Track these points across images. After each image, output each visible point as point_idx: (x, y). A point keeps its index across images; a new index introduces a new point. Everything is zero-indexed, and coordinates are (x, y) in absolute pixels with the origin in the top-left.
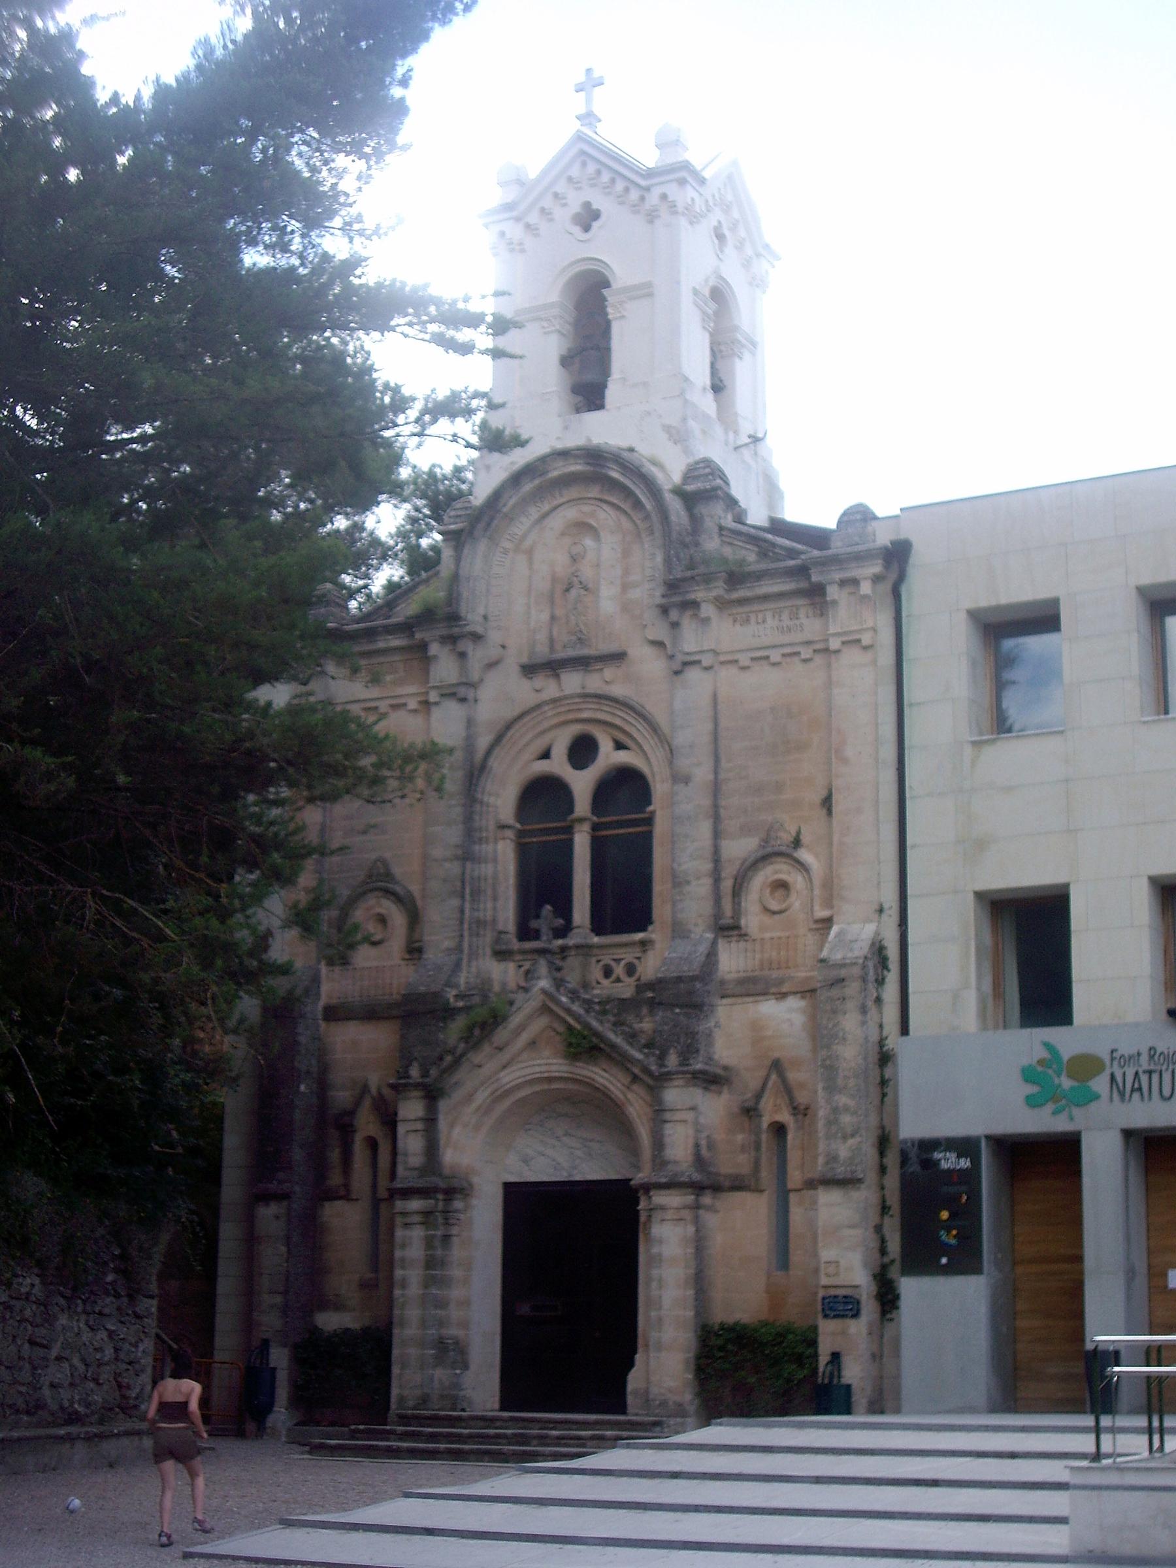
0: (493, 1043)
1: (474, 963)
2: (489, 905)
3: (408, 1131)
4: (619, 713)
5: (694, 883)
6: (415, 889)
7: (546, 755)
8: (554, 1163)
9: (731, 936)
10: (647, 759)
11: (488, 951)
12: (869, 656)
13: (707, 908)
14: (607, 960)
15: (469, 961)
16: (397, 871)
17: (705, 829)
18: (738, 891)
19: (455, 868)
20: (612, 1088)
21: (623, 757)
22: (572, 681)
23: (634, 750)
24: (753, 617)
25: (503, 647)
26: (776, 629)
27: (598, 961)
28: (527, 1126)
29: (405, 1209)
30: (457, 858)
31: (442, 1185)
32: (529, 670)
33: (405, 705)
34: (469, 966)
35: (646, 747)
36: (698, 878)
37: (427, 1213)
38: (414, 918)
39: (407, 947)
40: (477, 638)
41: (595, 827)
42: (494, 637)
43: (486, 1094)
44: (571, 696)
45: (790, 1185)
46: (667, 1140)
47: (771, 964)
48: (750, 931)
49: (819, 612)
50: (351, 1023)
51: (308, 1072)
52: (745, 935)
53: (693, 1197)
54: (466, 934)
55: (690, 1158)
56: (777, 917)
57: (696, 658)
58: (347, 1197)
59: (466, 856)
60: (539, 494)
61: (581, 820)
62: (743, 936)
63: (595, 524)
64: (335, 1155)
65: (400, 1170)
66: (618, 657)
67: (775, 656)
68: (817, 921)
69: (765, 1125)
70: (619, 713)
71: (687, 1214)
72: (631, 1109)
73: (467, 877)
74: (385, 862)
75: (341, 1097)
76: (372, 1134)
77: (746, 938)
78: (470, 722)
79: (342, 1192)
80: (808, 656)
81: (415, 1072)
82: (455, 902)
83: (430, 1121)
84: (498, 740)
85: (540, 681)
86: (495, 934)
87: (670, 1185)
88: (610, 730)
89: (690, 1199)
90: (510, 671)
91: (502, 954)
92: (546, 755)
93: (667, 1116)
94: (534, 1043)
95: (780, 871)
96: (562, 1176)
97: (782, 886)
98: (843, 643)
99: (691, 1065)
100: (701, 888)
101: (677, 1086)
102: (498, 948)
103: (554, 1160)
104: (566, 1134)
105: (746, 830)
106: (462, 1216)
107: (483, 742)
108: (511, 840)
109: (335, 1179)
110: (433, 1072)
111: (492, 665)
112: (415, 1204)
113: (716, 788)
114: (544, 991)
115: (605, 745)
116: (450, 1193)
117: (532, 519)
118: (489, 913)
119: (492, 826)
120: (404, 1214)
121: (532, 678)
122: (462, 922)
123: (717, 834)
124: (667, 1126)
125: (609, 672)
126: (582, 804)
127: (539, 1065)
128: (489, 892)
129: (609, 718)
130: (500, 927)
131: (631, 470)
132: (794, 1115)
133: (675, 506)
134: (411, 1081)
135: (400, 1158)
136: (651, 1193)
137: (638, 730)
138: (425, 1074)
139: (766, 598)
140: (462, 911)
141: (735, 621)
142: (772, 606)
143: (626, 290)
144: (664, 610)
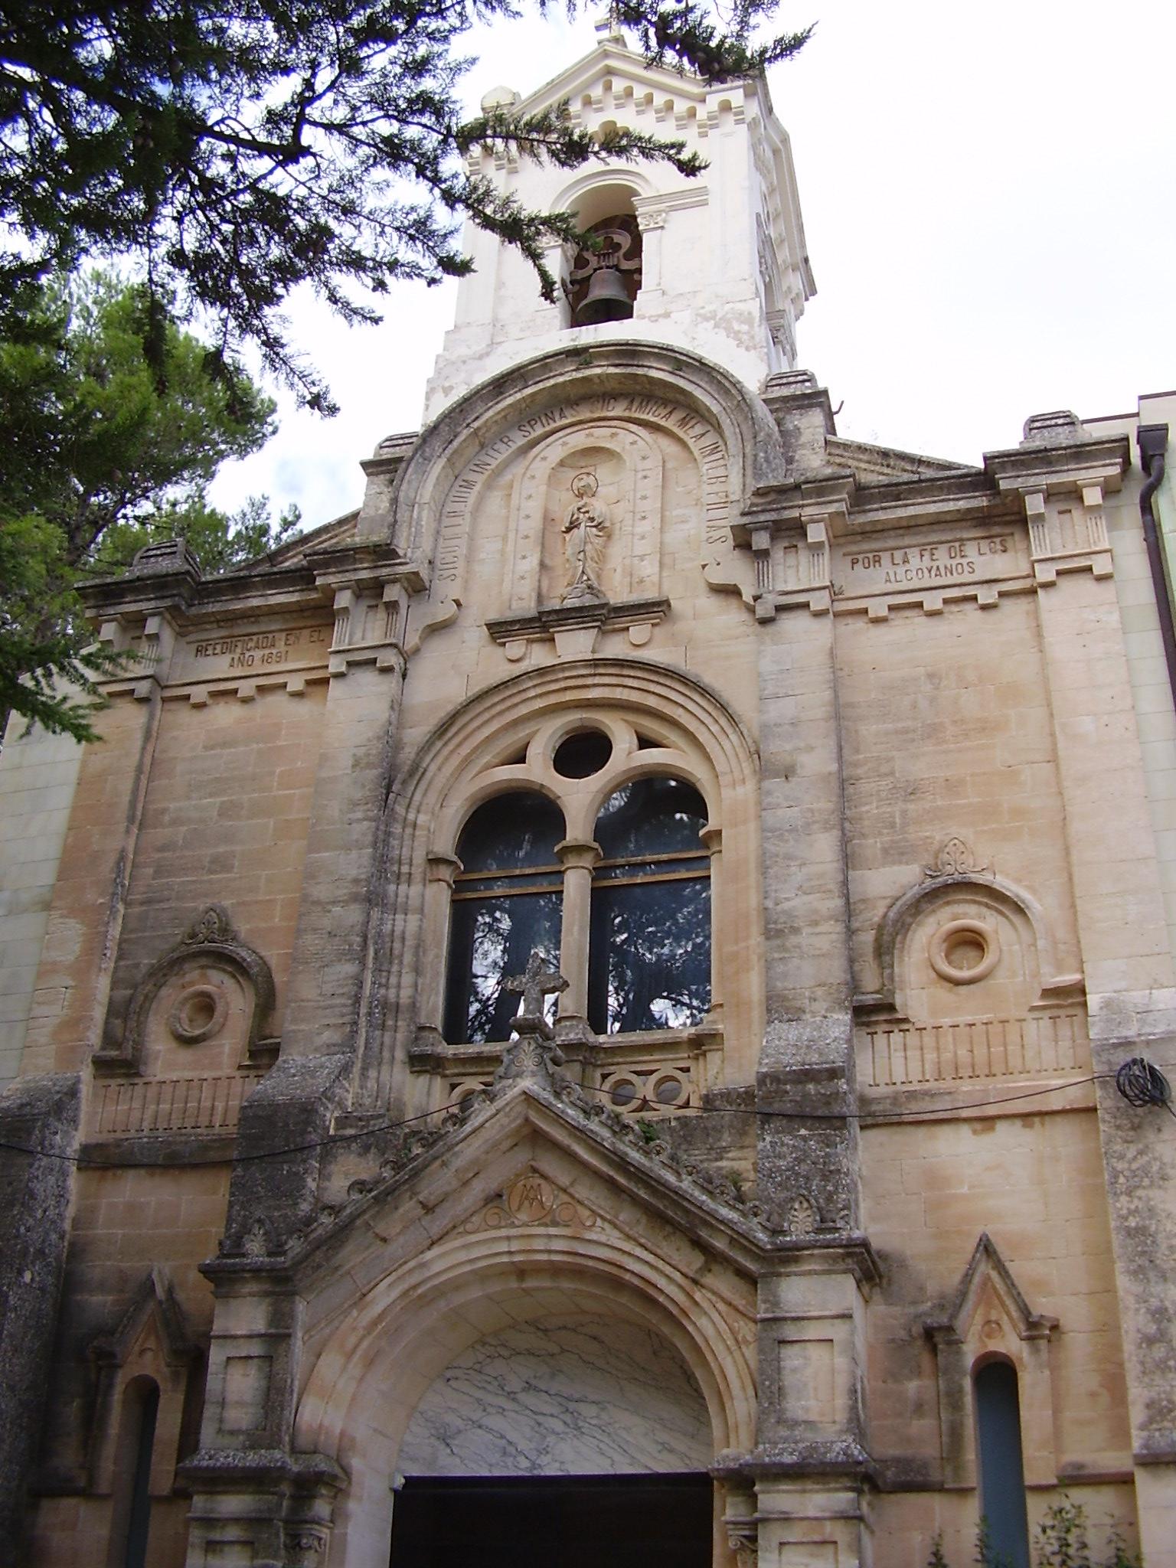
0: (417, 1194)
1: (372, 1073)
2: (407, 979)
3: (229, 1358)
4: (652, 687)
5: (806, 931)
6: (273, 955)
7: (520, 758)
8: (503, 1442)
9: (876, 1023)
10: (708, 758)
11: (400, 1055)
12: (1107, 590)
13: (836, 971)
14: (622, 1073)
15: (365, 1069)
16: (242, 927)
17: (824, 848)
18: (885, 949)
19: (353, 915)
20: (661, 1283)
21: (653, 757)
22: (575, 644)
23: (677, 748)
24: (885, 557)
25: (458, 604)
26: (926, 571)
27: (605, 1077)
28: (449, 1374)
29: (212, 1510)
30: (354, 898)
31: (294, 1465)
32: (500, 631)
33: (284, 686)
34: (364, 1075)
35: (703, 736)
36: (816, 923)
37: (254, 1522)
38: (266, 1004)
39: (251, 1042)
40: (417, 587)
41: (598, 873)
42: (447, 589)
43: (395, 1293)
44: (573, 664)
45: (1030, 1478)
46: (789, 1380)
47: (957, 1069)
48: (911, 1014)
49: (999, 547)
50: (131, 1174)
51: (41, 1253)
52: (905, 1020)
53: (852, 1495)
54: (363, 1021)
55: (842, 1416)
56: (963, 989)
57: (801, 598)
58: (87, 1493)
59: (373, 899)
60: (525, 415)
61: (579, 849)
62: (901, 1022)
63: (618, 450)
64: (72, 1411)
65: (208, 1433)
66: (655, 610)
67: (932, 601)
68: (1047, 993)
69: (969, 1360)
70: (652, 687)
71: (839, 1532)
72: (703, 1322)
73: (371, 933)
74: (222, 913)
75: (99, 1303)
76: (149, 1371)
77: (905, 1026)
78: (397, 706)
79: (82, 1483)
80: (990, 601)
81: (255, 1248)
82: (350, 968)
83: (277, 1339)
84: (442, 730)
85: (515, 648)
86: (413, 1028)
87: (800, 1473)
88: (632, 717)
89: (842, 1499)
90: (472, 636)
91: (422, 1063)
92: (520, 758)
93: (790, 1332)
94: (500, 1196)
95: (965, 915)
96: (520, 1468)
97: (970, 941)
98: (1059, 573)
99: (837, 1229)
100: (826, 939)
101: (810, 1273)
102: (416, 1050)
103: (502, 1437)
104: (529, 1387)
105: (896, 853)
106: (325, 1533)
107: (416, 734)
108: (449, 885)
109: (67, 1458)
110: (295, 1246)
111: (436, 629)
112: (233, 1504)
113: (844, 784)
114: (528, 1097)
115: (622, 739)
116: (307, 1486)
117: (514, 447)
118: (405, 994)
119: (419, 858)
120: (209, 1522)
121: (504, 644)
122: (357, 1000)
123: (848, 859)
124: (787, 1351)
125: (638, 632)
126: (578, 828)
127: (508, 1238)
128: (408, 958)
129: (635, 697)
130: (423, 1020)
131: (688, 365)
132: (1030, 1339)
133: (762, 411)
134: (246, 1261)
135: (210, 1412)
136: (757, 1488)
137: (689, 710)
138: (276, 1249)
139: (909, 527)
140: (360, 985)
141: (854, 562)
142: (921, 539)
143: (660, 198)
144: (743, 540)
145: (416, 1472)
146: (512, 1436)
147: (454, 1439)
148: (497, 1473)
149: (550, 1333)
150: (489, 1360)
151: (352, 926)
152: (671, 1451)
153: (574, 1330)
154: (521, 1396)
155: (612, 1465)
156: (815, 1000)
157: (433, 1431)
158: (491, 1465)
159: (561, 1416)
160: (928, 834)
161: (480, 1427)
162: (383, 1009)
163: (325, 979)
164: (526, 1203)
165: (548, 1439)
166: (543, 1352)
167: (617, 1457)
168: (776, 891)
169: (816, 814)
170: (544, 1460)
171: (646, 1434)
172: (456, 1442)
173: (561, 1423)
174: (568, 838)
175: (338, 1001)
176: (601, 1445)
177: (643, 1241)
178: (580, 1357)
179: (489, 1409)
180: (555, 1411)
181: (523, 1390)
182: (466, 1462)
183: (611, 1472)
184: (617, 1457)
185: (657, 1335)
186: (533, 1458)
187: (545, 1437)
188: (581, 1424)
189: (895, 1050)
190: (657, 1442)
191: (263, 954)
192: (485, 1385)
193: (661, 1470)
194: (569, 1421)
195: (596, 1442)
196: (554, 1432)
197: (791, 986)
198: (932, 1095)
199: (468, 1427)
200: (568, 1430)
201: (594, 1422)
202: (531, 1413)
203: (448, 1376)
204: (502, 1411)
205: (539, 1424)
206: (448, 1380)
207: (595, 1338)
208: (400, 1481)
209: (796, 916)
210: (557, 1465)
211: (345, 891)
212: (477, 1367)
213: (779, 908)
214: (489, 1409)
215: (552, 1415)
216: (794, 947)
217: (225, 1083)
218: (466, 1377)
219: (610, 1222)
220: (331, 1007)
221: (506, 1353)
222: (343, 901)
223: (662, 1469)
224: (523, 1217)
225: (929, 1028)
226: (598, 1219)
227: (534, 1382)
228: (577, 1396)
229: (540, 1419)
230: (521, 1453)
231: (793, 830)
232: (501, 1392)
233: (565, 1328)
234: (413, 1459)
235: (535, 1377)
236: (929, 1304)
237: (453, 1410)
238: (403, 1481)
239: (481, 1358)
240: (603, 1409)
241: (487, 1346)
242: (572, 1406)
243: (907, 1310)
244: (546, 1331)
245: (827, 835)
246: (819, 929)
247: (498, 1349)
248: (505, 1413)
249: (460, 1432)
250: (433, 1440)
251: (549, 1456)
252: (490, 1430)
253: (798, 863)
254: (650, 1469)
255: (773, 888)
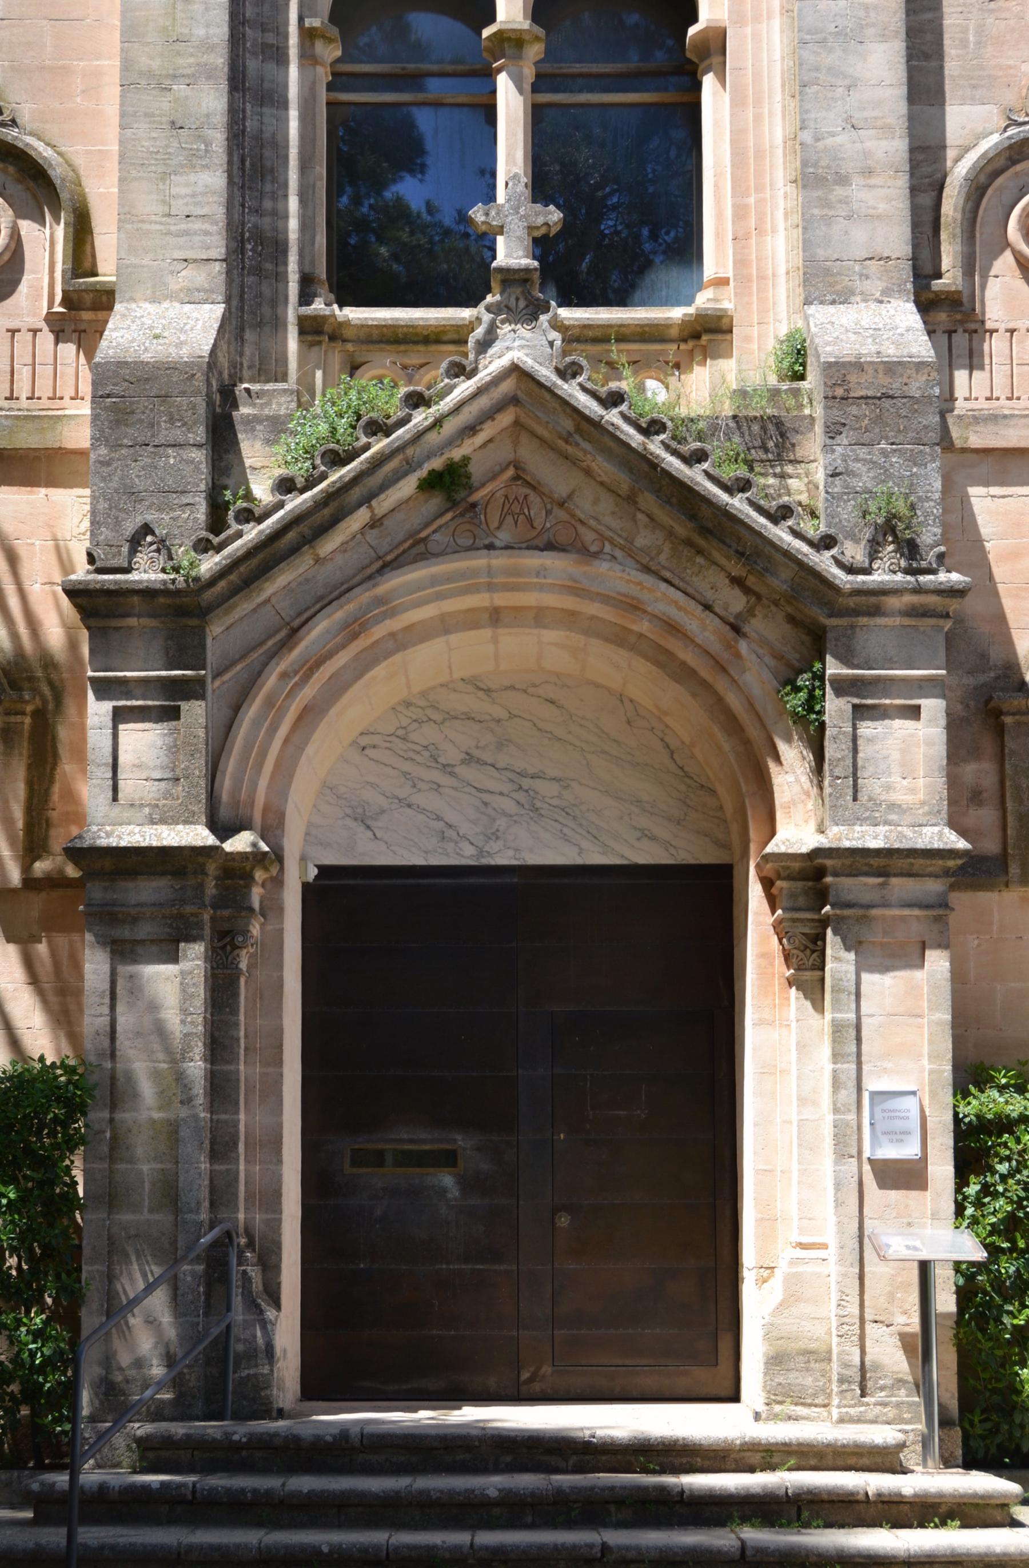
5: (857, 181)
8: (440, 825)
41: (542, 82)
96: (464, 855)
103: (439, 818)
145: (332, 858)
146: (451, 817)
147: (376, 820)
148: (435, 861)
149: (494, 695)
150: (415, 725)
151: (208, 116)
152: (653, 838)
153: (525, 691)
154: (461, 770)
155: (579, 854)
156: (867, 277)
157: (349, 811)
158: (426, 852)
159: (514, 795)
160: (1011, 62)
161: (409, 806)
162: (256, 244)
163: (173, 192)
164: (509, 520)
165: (498, 822)
166: (488, 717)
167: (585, 844)
168: (816, 120)
169: (872, 14)
170: (494, 846)
171: (621, 818)
172: (380, 824)
173: (513, 803)
174: (501, 14)
175: (197, 225)
176: (565, 830)
177: (667, 575)
178: (535, 725)
179: (421, 785)
180: (506, 788)
181: (463, 762)
182: (393, 848)
183: (579, 861)
184: (585, 844)
185: (631, 701)
186: (480, 844)
187: (494, 820)
188: (539, 804)
189: (959, 356)
190: (635, 828)
191: (63, 149)
192: (414, 756)
193: (642, 861)
194: (523, 800)
195: (559, 827)
196: (505, 814)
197: (836, 256)
198: (994, 418)
199: (394, 806)
200: (523, 812)
201: (555, 802)
202: (473, 791)
203: (363, 744)
204: (437, 787)
205: (486, 804)
206: (364, 749)
207: (552, 702)
208: (313, 872)
209: (844, 159)
210: (511, 853)
211: (192, 60)
212: (400, 732)
213: (820, 145)
214: (421, 785)
215: (501, 794)
216: (840, 201)
217: (26, 337)
218: (388, 745)
219: (622, 548)
220: (186, 233)
221: (437, 717)
222: (188, 76)
223: (642, 860)
224: (503, 537)
225: (1002, 330)
226: (607, 544)
227: (476, 753)
228: (531, 770)
229: (486, 797)
230: (464, 837)
231: (840, 34)
232: (434, 765)
233: (513, 688)
234: (325, 845)
235: (477, 747)
236: (992, 674)
237: (372, 785)
238: (316, 871)
239: (405, 722)
240: (566, 787)
241: (411, 708)
242: (526, 783)
243: (965, 681)
244: (488, 691)
245: (884, 46)
246: (873, 181)
247: (429, 712)
248: (441, 790)
249: (383, 812)
250: (349, 822)
251: (500, 843)
252: (423, 810)
253: (847, 82)
254: (626, 858)
255: (813, 116)
